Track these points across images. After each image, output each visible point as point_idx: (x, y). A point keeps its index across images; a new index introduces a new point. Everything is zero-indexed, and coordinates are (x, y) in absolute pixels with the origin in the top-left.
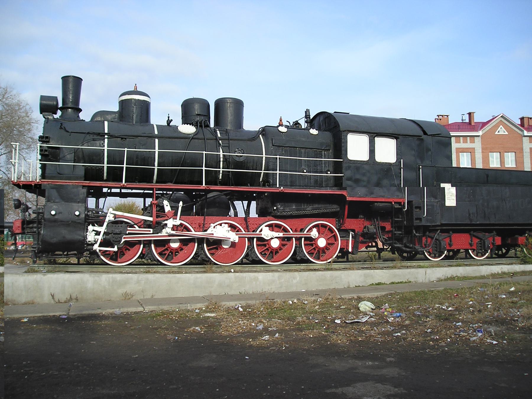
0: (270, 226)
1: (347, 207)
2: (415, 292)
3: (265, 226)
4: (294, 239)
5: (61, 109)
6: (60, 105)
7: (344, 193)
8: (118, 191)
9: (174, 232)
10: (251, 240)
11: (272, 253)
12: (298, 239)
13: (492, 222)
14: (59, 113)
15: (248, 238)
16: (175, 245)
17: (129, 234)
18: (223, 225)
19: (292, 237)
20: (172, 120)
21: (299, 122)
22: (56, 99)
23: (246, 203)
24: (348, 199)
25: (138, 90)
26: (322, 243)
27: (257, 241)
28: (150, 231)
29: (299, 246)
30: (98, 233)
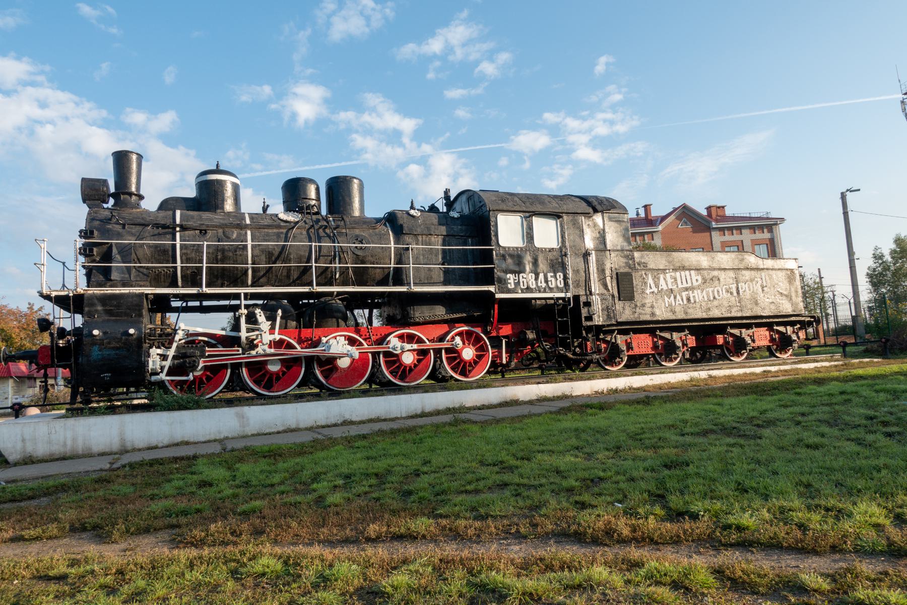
0: (401, 337)
1: (496, 306)
2: (294, 443)
3: (394, 337)
4: (432, 351)
5: (113, 195)
6: (112, 189)
7: (492, 289)
8: (197, 304)
9: (272, 351)
10: (438, 352)
11: (404, 372)
12: (438, 352)
13: (744, 315)
14: (112, 201)
15: (371, 352)
16: (274, 368)
17: (210, 356)
18: (338, 338)
19: (429, 349)
20: (268, 206)
21: (436, 205)
22: (105, 182)
23: (367, 311)
24: (498, 296)
25: (221, 168)
26: (468, 353)
27: (384, 357)
28: (238, 351)
29: (376, 364)
30: (164, 357)
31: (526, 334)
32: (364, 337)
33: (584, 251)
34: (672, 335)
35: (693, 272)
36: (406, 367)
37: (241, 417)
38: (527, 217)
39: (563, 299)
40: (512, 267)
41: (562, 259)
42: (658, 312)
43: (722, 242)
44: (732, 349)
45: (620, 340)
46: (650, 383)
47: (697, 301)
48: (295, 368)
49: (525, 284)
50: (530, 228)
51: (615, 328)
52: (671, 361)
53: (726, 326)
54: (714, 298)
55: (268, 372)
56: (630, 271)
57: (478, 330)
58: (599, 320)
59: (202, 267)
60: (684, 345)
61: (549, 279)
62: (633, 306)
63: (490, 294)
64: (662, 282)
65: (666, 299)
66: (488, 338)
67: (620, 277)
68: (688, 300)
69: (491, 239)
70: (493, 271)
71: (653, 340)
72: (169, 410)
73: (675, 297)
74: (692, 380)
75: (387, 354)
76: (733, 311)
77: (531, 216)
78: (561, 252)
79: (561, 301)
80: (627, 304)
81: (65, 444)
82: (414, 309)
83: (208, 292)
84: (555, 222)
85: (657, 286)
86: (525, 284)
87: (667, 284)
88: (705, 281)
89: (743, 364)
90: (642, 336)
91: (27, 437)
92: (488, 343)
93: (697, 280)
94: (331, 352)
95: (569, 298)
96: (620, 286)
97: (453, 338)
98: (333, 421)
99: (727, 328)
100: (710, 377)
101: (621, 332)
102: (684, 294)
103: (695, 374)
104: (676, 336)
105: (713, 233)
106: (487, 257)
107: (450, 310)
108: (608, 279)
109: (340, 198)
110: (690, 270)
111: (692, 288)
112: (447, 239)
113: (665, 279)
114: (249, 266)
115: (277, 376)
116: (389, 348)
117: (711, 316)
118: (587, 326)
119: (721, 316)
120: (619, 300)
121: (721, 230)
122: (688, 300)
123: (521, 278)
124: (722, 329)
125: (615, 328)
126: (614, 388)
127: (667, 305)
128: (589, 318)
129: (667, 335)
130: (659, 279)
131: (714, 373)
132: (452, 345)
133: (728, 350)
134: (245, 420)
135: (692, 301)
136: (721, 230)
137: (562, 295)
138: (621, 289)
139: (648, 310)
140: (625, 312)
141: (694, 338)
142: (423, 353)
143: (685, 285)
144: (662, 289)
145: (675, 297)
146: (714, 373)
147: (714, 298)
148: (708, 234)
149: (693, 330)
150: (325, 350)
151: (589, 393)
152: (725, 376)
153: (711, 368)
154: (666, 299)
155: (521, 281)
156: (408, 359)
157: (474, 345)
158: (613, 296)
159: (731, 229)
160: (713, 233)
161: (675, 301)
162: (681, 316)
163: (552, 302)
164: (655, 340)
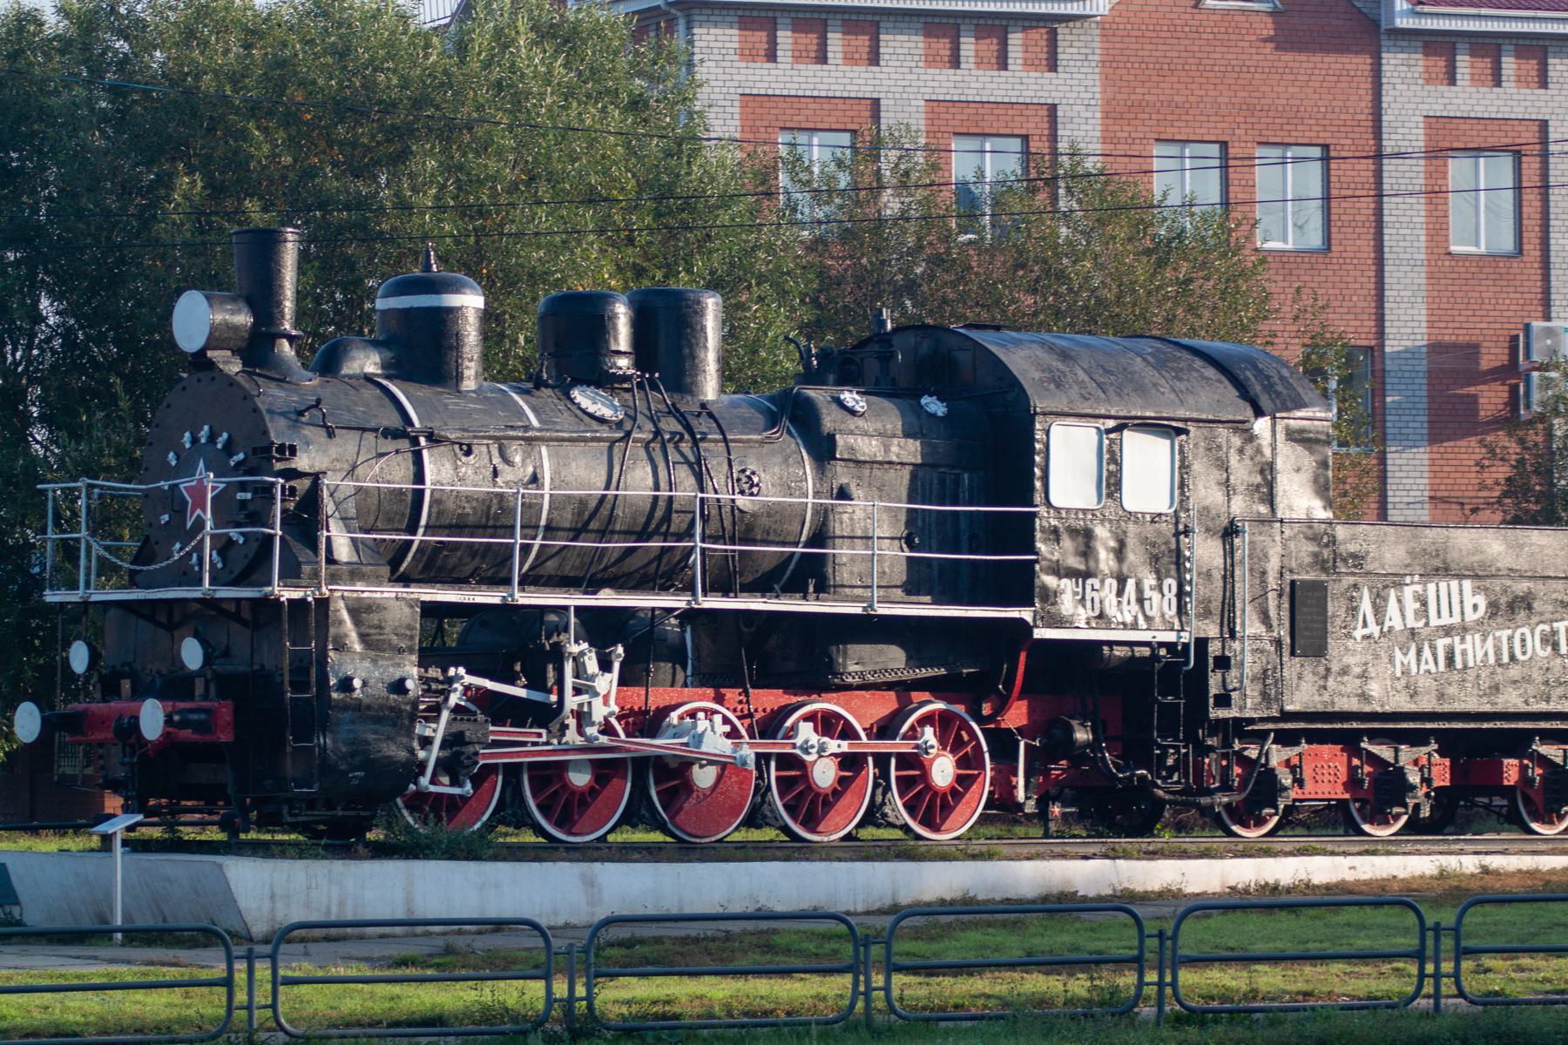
4: (870, 759)
7: (1026, 614)
16: (580, 779)
19: (865, 755)
24: (1040, 633)
26: (943, 771)
28: (540, 735)
31: (1071, 731)
32: (739, 714)
33: (1226, 522)
34: (1397, 751)
35: (1467, 584)
36: (818, 795)
37: (589, 883)
38: (1109, 431)
39: (1170, 646)
40: (1074, 562)
41: (1178, 542)
42: (1374, 689)
43: (1434, 122)
44: (1538, 800)
45: (1277, 755)
46: (1350, 876)
47: (1471, 664)
48: (615, 781)
49: (1097, 605)
50: (1115, 459)
51: (1270, 726)
52: (1385, 822)
53: (1528, 735)
54: (1512, 658)
55: (566, 785)
56: (1323, 577)
57: (960, 709)
58: (1248, 705)
59: (513, 545)
60: (1426, 781)
61: (1147, 594)
62: (1321, 670)
63: (1022, 627)
64: (1392, 608)
65: (1398, 655)
66: (983, 731)
67: (1298, 593)
68: (1450, 659)
69: (1032, 488)
70: (1033, 572)
71: (1349, 762)
72: (453, 857)
73: (1419, 652)
74: (1443, 875)
75: (787, 761)
76: (1554, 698)
77: (1119, 429)
78: (1177, 523)
79: (1163, 652)
80: (1309, 664)
81: (328, 912)
82: (845, 652)
83: (522, 601)
84: (1167, 442)
85: (1380, 623)
86: (1097, 605)
87: (1404, 619)
88: (1493, 607)
89: (1560, 846)
90: (1327, 750)
91: (278, 891)
92: (985, 748)
93: (1475, 607)
94: (704, 749)
95: (1186, 646)
96: (1298, 617)
97: (913, 734)
98: (736, 908)
99: (1533, 741)
100: (1485, 870)
101: (1286, 739)
102: (1441, 643)
103: (1451, 862)
104: (1407, 754)
105: (1395, 64)
106: (1020, 533)
107: (914, 659)
108: (1272, 596)
109: (687, 351)
110: (1460, 577)
111: (1464, 629)
112: (920, 474)
113: (1399, 601)
114: (519, 541)
115: (585, 798)
116: (794, 746)
117: (1499, 708)
118: (1218, 721)
119: (1523, 708)
120: (1293, 654)
121: (1441, 46)
122: (1450, 659)
123: (1088, 588)
124: (1518, 743)
125: (1270, 726)
126: (1271, 881)
127: (1398, 674)
128: (1224, 700)
129: (1384, 752)
130: (1386, 600)
131: (1496, 862)
132: (917, 746)
133: (1528, 801)
134: (595, 890)
135: (1459, 665)
136: (1441, 46)
137: (1171, 637)
138: (1299, 624)
139: (1352, 684)
140: (1302, 696)
141: (1447, 762)
142: (850, 763)
143: (1446, 620)
144: (1391, 629)
145: (1419, 652)
146: (1496, 862)
147: (1512, 658)
148: (1362, 63)
149: (1450, 743)
150: (686, 744)
151: (1218, 889)
152: (1520, 871)
153: (1480, 848)
154: (1398, 655)
155: (1088, 597)
156: (825, 774)
157: (952, 752)
158: (1278, 643)
159: (1488, 46)
160: (1395, 64)
161: (1419, 661)
162: (1427, 704)
163: (1146, 651)
164: (1356, 762)
